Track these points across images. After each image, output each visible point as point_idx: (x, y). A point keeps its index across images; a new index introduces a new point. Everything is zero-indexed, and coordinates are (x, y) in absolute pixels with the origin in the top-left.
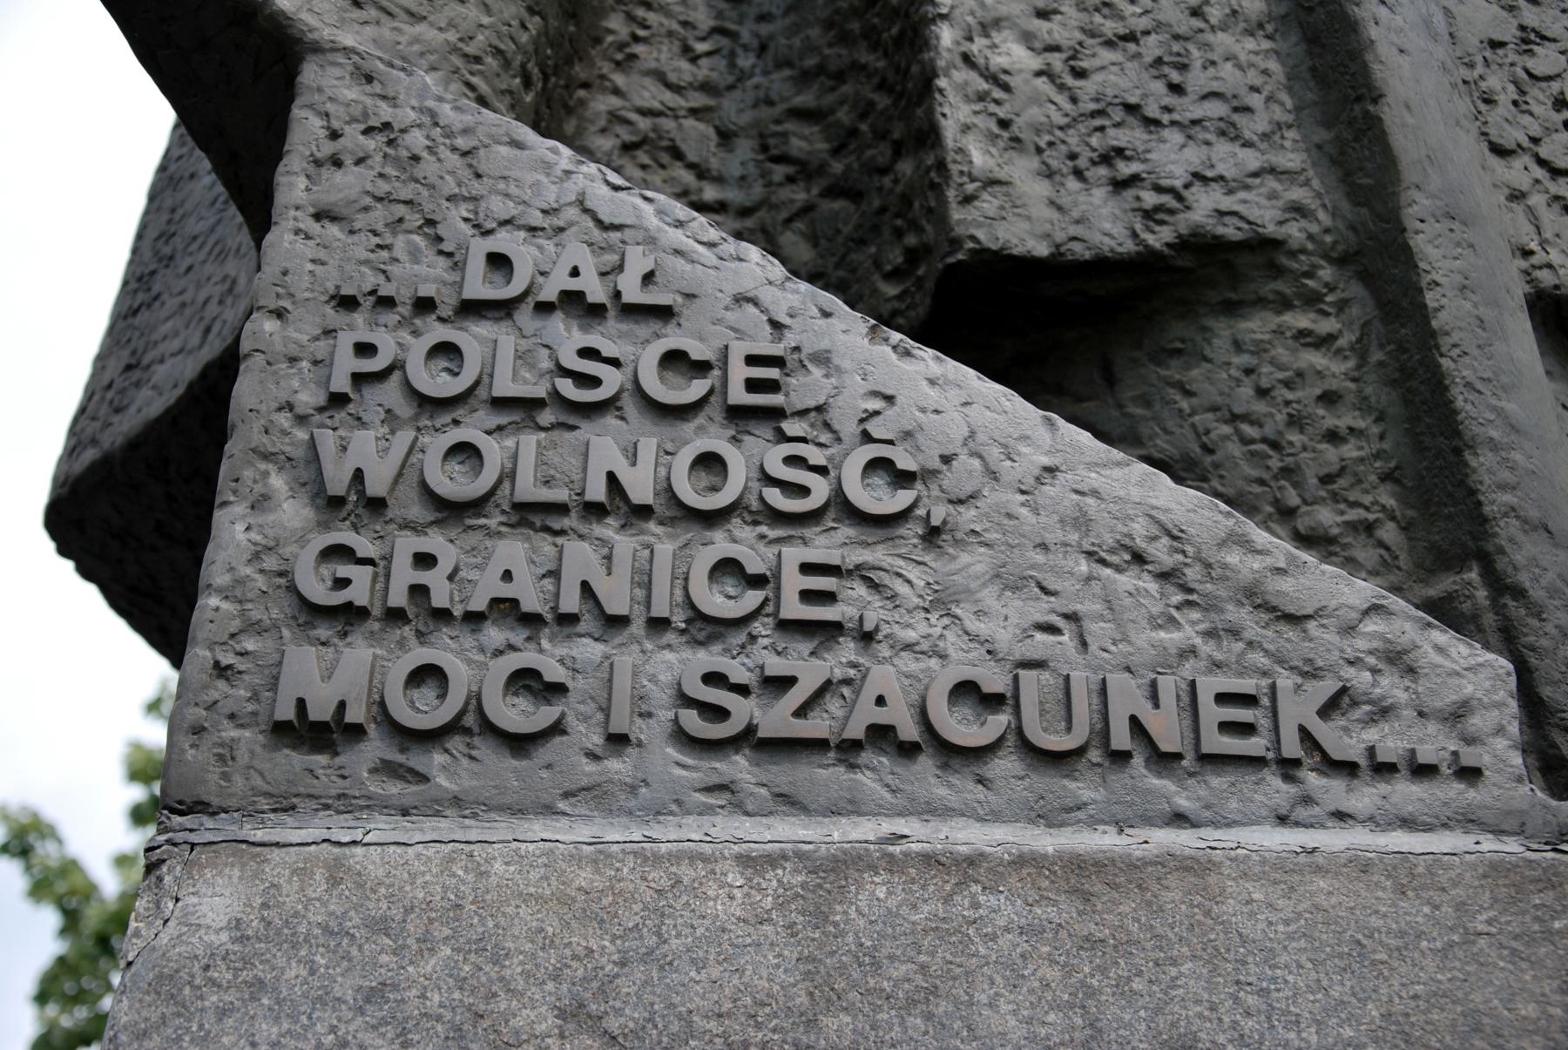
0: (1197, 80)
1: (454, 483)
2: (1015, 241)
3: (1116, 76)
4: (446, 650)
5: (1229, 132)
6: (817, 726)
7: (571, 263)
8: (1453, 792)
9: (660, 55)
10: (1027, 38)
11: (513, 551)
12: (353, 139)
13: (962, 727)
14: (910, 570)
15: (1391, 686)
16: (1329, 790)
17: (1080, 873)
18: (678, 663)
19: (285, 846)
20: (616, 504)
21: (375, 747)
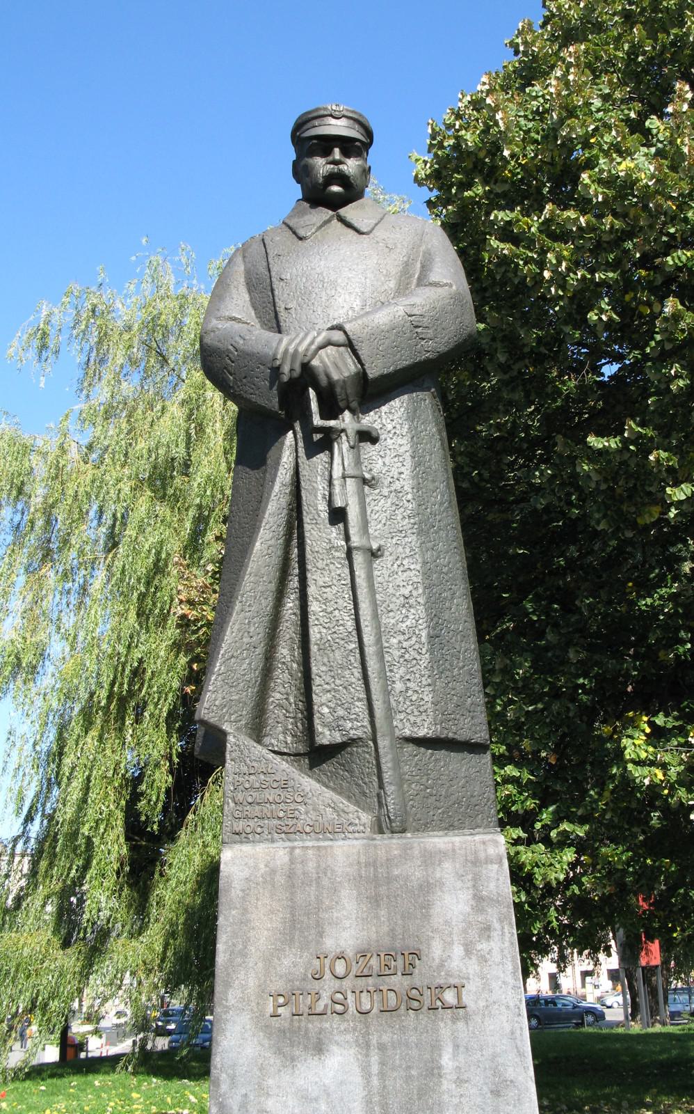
0: (353, 711)
1: (250, 800)
2: (219, 1066)
3: (341, 712)
4: (251, 823)
5: (356, 720)
6: (292, 830)
7: (262, 767)
8: (362, 835)
9: (281, 689)
10: (327, 706)
11: (257, 808)
12: (234, 747)
13: (308, 829)
14: (302, 808)
15: (357, 821)
16: (350, 836)
17: (319, 848)
18: (276, 822)
19: (290, 228)
20: (268, 802)
21: (244, 835)
